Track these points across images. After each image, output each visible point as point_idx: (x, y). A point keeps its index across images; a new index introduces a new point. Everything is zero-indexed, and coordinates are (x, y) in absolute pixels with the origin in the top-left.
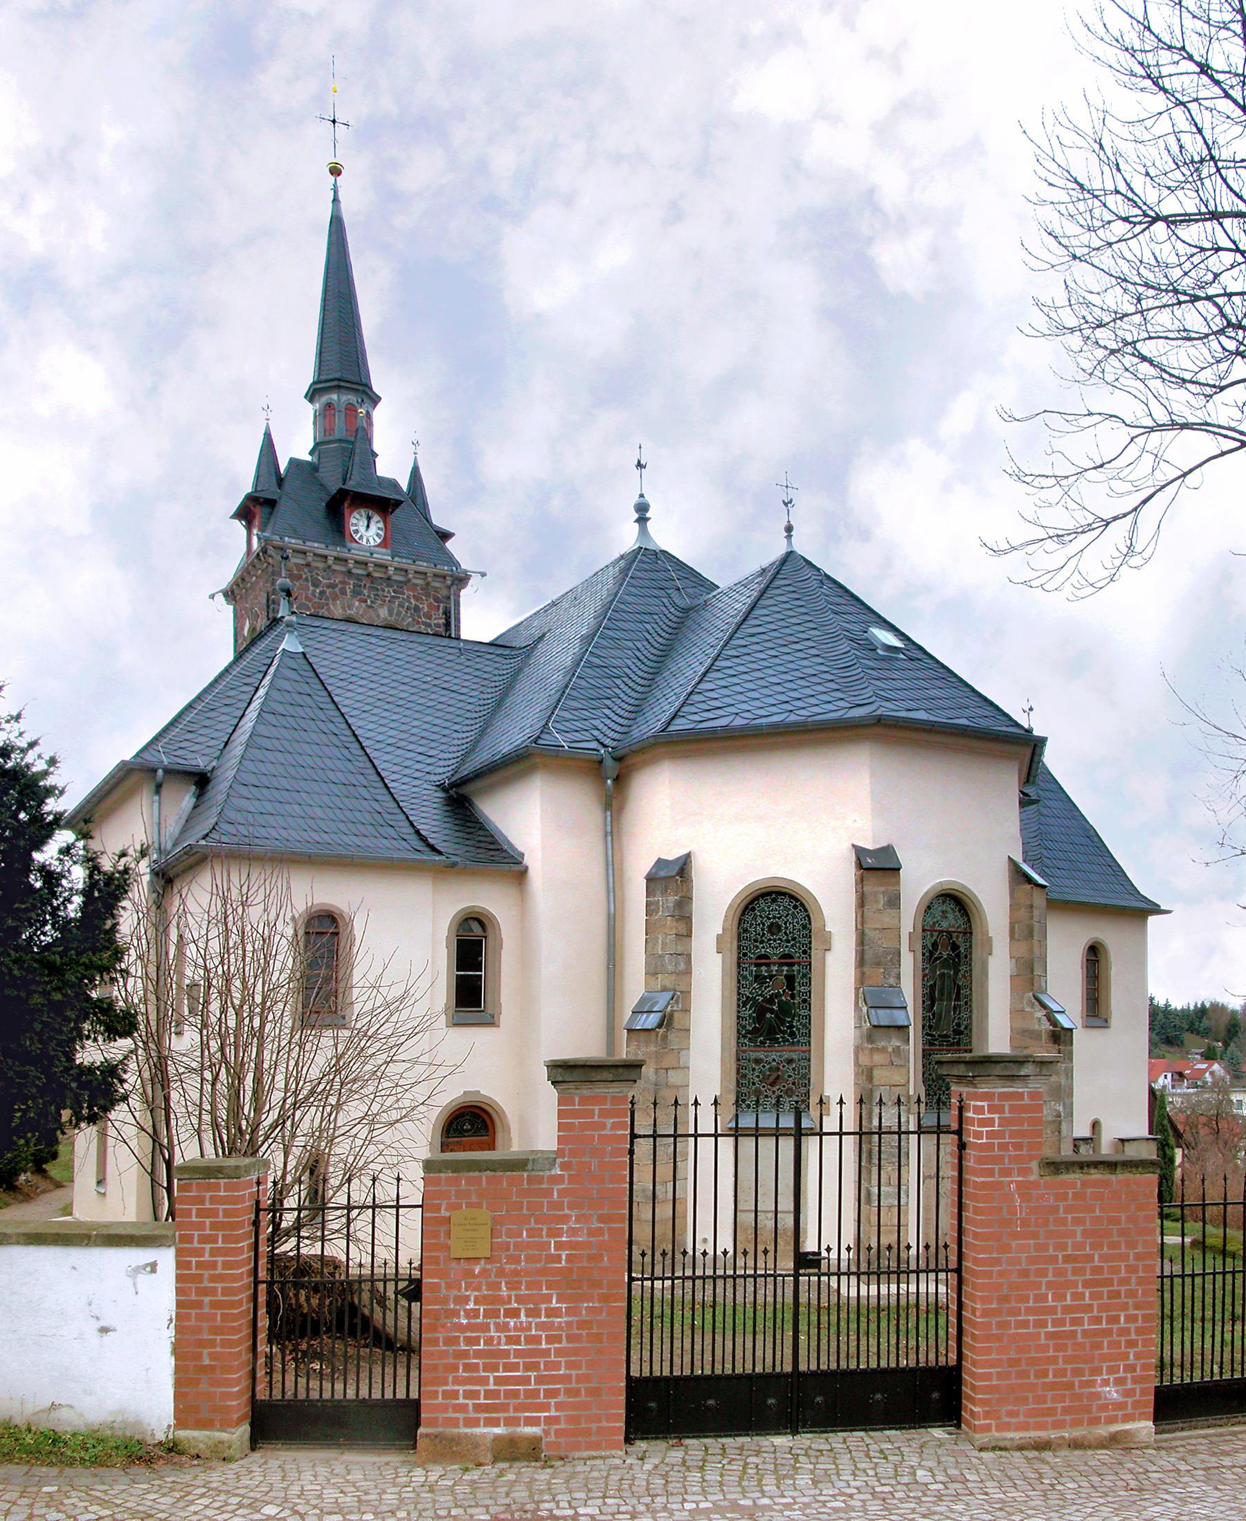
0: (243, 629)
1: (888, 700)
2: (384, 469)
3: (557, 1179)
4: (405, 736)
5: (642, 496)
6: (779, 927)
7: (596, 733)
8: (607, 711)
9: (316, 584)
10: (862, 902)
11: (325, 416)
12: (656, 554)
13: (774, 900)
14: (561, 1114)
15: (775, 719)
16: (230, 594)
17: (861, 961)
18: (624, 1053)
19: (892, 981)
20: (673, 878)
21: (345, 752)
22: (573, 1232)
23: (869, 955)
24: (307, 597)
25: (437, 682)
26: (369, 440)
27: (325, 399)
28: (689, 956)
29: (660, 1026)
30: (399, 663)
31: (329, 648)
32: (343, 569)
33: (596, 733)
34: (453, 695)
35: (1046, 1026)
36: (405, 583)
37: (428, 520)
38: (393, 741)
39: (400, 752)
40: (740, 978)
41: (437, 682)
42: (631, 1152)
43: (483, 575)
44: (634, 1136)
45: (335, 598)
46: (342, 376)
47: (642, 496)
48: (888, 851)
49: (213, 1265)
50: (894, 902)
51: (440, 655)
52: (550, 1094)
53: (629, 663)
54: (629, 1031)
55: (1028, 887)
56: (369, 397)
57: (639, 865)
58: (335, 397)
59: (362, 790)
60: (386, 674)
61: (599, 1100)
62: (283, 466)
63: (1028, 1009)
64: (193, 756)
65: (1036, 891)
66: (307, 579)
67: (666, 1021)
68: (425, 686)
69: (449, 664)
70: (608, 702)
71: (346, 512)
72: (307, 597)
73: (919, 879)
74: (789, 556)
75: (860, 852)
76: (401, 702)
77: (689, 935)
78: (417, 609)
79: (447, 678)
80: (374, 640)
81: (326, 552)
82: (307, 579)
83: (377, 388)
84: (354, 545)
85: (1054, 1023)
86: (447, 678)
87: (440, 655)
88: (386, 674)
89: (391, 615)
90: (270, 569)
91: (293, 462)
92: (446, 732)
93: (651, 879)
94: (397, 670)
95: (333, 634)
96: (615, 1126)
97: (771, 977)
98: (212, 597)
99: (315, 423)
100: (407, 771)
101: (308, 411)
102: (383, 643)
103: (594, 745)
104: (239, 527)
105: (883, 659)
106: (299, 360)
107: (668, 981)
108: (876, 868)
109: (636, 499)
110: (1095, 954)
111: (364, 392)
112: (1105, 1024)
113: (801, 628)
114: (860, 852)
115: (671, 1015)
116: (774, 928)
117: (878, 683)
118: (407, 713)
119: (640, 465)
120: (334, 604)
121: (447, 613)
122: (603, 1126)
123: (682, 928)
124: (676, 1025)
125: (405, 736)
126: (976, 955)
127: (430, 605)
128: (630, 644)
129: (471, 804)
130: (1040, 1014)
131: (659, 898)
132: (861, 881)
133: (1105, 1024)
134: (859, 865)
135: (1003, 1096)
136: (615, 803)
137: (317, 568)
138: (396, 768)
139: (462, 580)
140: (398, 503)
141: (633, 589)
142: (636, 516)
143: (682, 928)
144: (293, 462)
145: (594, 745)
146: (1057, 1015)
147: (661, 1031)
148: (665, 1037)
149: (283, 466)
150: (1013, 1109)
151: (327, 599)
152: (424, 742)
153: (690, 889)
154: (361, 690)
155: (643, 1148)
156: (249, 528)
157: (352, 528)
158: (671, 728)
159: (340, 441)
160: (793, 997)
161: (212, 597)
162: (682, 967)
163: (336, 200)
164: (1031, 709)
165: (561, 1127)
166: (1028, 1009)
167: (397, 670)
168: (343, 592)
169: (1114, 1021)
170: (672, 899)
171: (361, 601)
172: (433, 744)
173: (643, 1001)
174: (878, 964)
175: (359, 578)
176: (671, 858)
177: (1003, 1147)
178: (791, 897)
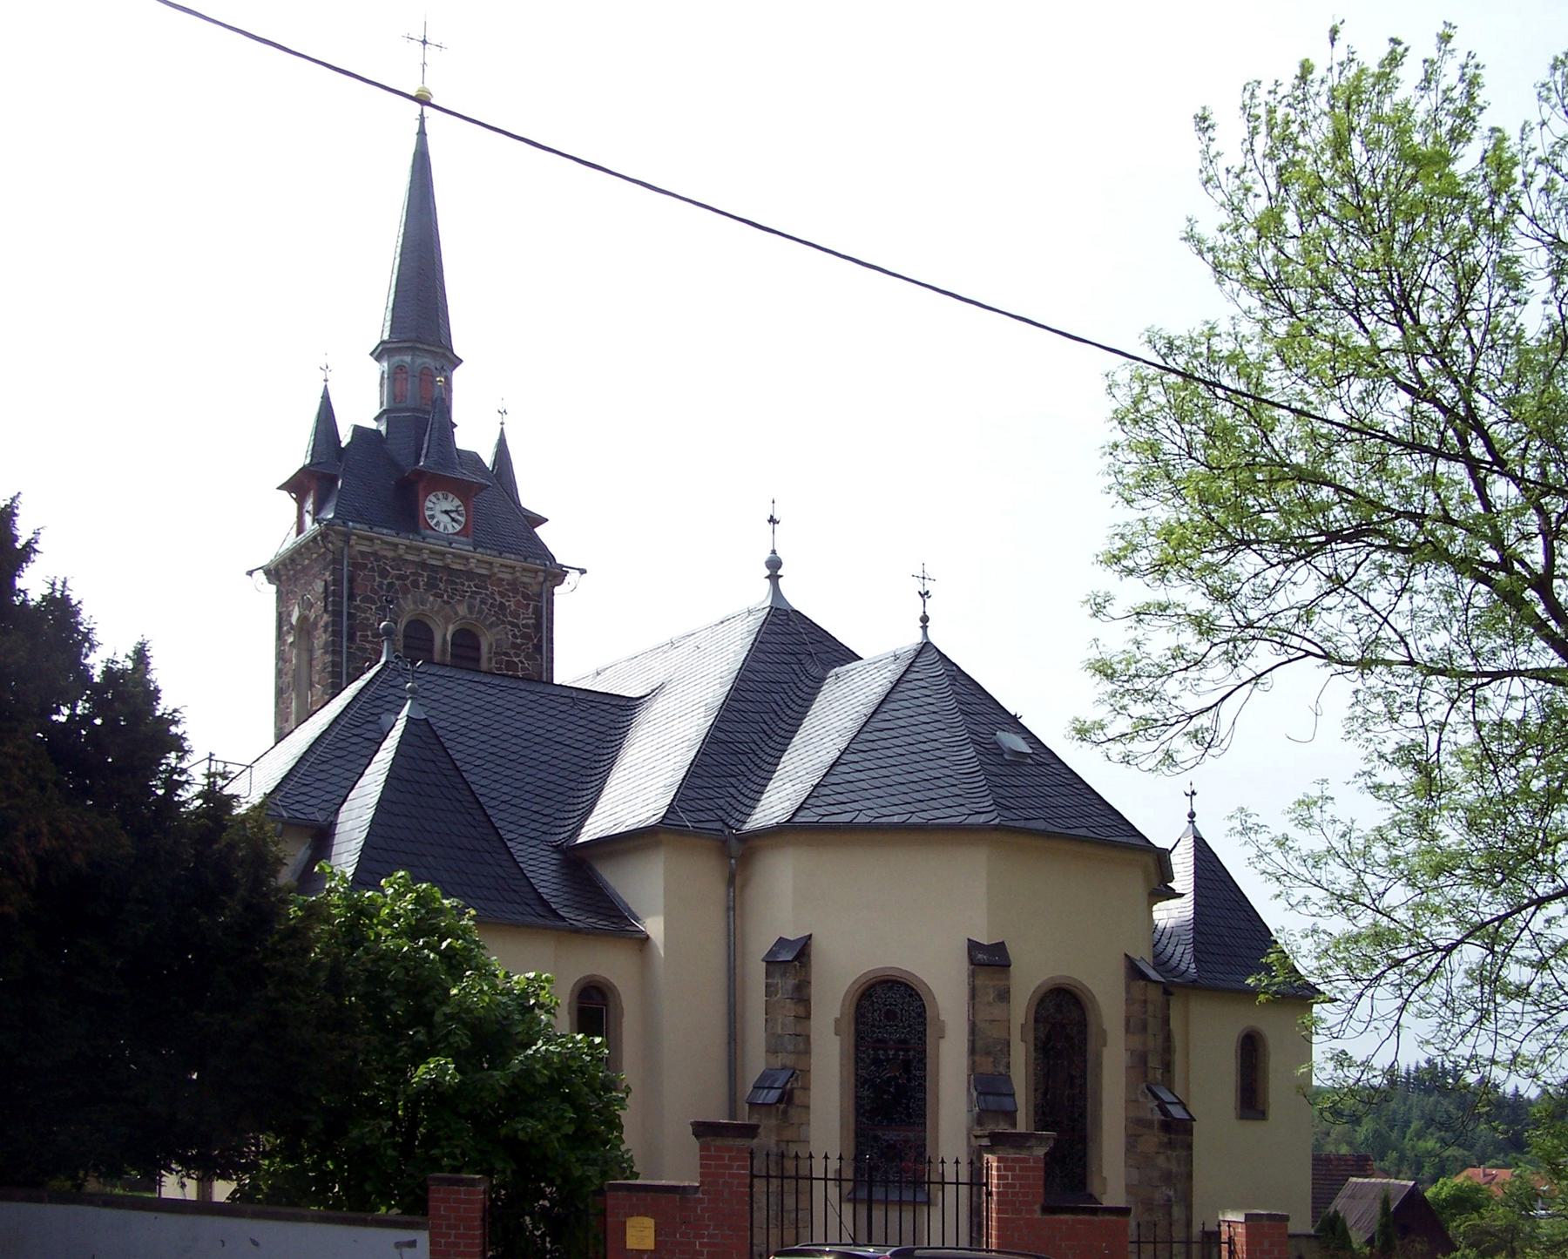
0: (290, 615)
1: (1008, 808)
2: (464, 439)
3: (700, 1201)
4: (519, 793)
5: (774, 552)
6: (895, 1014)
7: (720, 813)
8: (732, 790)
9: (384, 574)
10: (973, 994)
11: (395, 380)
12: (788, 615)
13: (891, 988)
14: (702, 1158)
15: (896, 819)
16: (274, 573)
17: (973, 1051)
18: (744, 1119)
19: (1002, 1069)
20: (793, 959)
21: (469, 818)
22: (710, 1236)
23: (979, 1044)
24: (372, 589)
25: (549, 735)
26: (446, 409)
27: (397, 359)
28: (808, 1037)
29: (780, 1100)
30: (509, 713)
31: (436, 697)
32: (417, 559)
33: (720, 813)
34: (566, 749)
35: (1158, 1116)
36: (489, 577)
37: (517, 503)
38: (507, 798)
39: (513, 810)
40: (858, 1060)
41: (549, 735)
42: (751, 1186)
43: (583, 572)
44: (753, 1176)
45: (406, 591)
46: (419, 329)
47: (774, 552)
48: (999, 949)
49: (457, 1245)
50: (1004, 996)
51: (552, 704)
52: (694, 1143)
53: (756, 737)
54: (752, 1105)
55: (1142, 983)
56: (450, 361)
57: (760, 944)
58: (408, 359)
59: (487, 856)
60: (496, 726)
61: (730, 1149)
62: (345, 437)
63: (1141, 1099)
64: (311, 810)
65: (1151, 986)
66: (372, 569)
67: (786, 1097)
68: (537, 740)
69: (561, 716)
70: (732, 780)
71: (421, 494)
72: (372, 589)
73: (1031, 973)
74: (926, 646)
75: (973, 946)
76: (513, 757)
77: (808, 1017)
78: (502, 606)
79: (560, 731)
80: (482, 688)
81: (396, 540)
82: (372, 569)
83: (458, 349)
84: (429, 532)
85: (1165, 1112)
86: (560, 731)
87: (552, 704)
88: (496, 726)
89: (471, 612)
90: (330, 556)
91: (358, 431)
92: (561, 790)
93: (771, 962)
94: (507, 721)
95: (441, 681)
96: (739, 1168)
97: (888, 1060)
98: (250, 573)
99: (381, 385)
100: (522, 830)
101: (375, 371)
102: (491, 691)
103: (718, 825)
104: (288, 503)
105: (1011, 764)
106: (371, 312)
107: (789, 1060)
108: (989, 961)
109: (767, 555)
110: (1251, 1049)
111: (444, 355)
112: (1262, 1115)
113: (928, 727)
114: (973, 946)
115: (792, 1090)
116: (890, 1015)
117: (1000, 791)
118: (520, 768)
119: (772, 520)
120: (405, 598)
121: (538, 612)
122: (731, 1167)
123: (801, 1011)
124: (797, 1101)
125: (519, 793)
126: (1091, 1046)
127: (518, 603)
128: (757, 717)
129: (591, 868)
130: (1154, 1104)
131: (777, 980)
132: (973, 975)
133: (1262, 1115)
134: (972, 960)
135: (1014, 1160)
136: (738, 881)
137: (385, 557)
138: (512, 827)
139: (558, 574)
140: (483, 487)
141: (761, 655)
142: (768, 572)
143: (801, 1011)
144: (358, 431)
145: (718, 825)
146: (1169, 1107)
147: (782, 1106)
148: (785, 1112)
149: (345, 437)
150: (1021, 1169)
151: (396, 592)
152: (538, 799)
153: (808, 974)
154: (472, 743)
155: (759, 1185)
156: (300, 502)
157: (428, 513)
158: (796, 819)
159: (413, 410)
160: (909, 1080)
161: (250, 573)
162: (802, 1046)
163: (422, 133)
164: (1193, 793)
165: (702, 1166)
166: (1141, 1099)
167: (507, 721)
168: (415, 584)
169: (1273, 1112)
170: (791, 982)
171: (435, 595)
172: (548, 803)
173: (763, 1076)
174: (988, 1054)
175: (434, 568)
176: (791, 938)
177: (1014, 1194)
178: (907, 986)
